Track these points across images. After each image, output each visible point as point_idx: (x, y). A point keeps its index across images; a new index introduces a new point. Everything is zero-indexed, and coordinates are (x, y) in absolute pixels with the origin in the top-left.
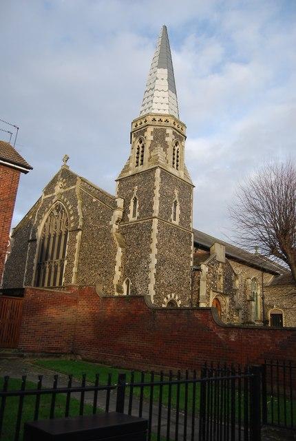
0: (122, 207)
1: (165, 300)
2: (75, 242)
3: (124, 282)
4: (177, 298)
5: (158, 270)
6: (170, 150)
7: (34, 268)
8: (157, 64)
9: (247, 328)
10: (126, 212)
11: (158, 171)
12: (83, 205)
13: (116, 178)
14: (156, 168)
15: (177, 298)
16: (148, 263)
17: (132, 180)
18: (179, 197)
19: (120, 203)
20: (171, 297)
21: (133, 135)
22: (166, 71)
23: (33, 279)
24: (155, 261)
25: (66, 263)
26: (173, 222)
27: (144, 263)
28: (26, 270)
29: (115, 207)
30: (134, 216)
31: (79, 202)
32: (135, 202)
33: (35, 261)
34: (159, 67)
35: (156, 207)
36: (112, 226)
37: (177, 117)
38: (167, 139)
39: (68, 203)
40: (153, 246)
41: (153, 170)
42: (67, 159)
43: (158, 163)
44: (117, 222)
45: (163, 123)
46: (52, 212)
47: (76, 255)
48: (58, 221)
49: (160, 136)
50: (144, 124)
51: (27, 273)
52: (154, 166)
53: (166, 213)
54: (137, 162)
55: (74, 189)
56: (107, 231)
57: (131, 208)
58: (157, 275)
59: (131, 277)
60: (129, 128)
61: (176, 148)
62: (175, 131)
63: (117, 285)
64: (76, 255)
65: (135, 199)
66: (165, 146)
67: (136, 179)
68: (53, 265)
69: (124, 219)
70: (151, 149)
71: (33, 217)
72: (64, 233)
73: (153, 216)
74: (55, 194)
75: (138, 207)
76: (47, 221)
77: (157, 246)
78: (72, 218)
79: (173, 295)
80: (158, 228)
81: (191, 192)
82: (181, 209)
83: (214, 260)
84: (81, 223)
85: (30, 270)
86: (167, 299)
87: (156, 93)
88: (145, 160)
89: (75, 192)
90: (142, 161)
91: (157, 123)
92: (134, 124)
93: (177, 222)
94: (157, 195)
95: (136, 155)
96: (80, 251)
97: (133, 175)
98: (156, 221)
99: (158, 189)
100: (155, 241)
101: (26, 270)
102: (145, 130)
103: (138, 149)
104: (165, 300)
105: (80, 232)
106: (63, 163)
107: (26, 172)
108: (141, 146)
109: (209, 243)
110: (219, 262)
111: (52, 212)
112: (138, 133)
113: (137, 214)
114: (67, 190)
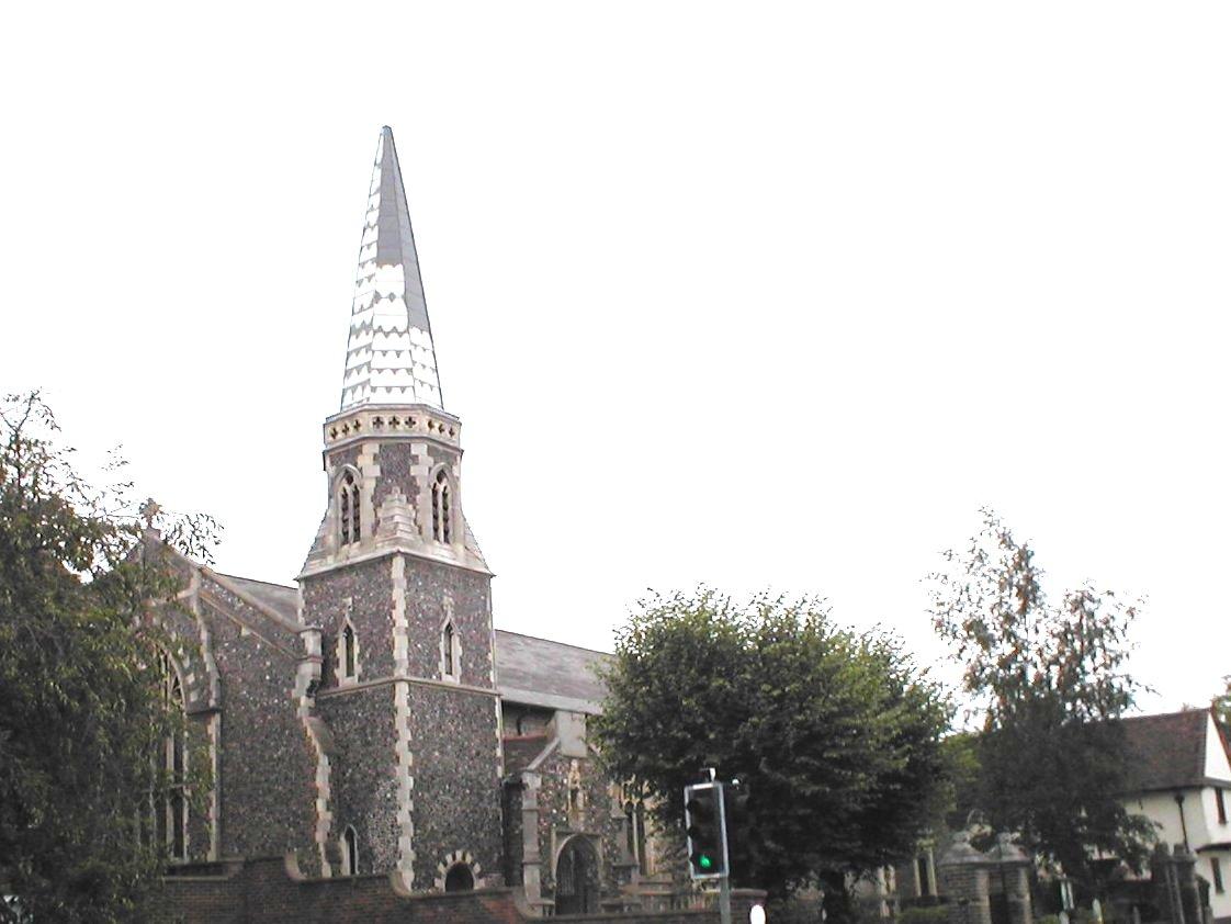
3: (343, 838)
4: (469, 859)
6: (424, 498)
8: (373, 252)
10: (328, 663)
14: (391, 556)
15: (469, 859)
16: (394, 788)
18: (455, 613)
19: (312, 644)
21: (328, 462)
24: (410, 782)
26: (448, 680)
27: (384, 786)
29: (300, 654)
30: (350, 673)
34: (380, 261)
35: (401, 651)
38: (414, 471)
40: (402, 747)
43: (397, 541)
44: (309, 691)
45: (402, 429)
49: (396, 459)
53: (424, 661)
56: (288, 714)
57: (341, 652)
58: (415, 816)
60: (317, 444)
61: (441, 488)
62: (431, 444)
63: (326, 846)
65: (348, 631)
66: (411, 489)
67: (346, 580)
69: (325, 679)
70: (377, 502)
75: (357, 650)
78: (191, 679)
79: (459, 854)
80: (410, 703)
82: (464, 643)
83: (554, 754)
86: (445, 864)
90: (357, 530)
91: (386, 430)
92: (329, 430)
93: (453, 680)
94: (402, 622)
97: (339, 571)
99: (401, 607)
100: (405, 735)
102: (359, 451)
103: (345, 496)
104: (441, 868)
105: (218, 717)
108: (349, 489)
110: (570, 758)
112: (340, 457)
113: (358, 669)
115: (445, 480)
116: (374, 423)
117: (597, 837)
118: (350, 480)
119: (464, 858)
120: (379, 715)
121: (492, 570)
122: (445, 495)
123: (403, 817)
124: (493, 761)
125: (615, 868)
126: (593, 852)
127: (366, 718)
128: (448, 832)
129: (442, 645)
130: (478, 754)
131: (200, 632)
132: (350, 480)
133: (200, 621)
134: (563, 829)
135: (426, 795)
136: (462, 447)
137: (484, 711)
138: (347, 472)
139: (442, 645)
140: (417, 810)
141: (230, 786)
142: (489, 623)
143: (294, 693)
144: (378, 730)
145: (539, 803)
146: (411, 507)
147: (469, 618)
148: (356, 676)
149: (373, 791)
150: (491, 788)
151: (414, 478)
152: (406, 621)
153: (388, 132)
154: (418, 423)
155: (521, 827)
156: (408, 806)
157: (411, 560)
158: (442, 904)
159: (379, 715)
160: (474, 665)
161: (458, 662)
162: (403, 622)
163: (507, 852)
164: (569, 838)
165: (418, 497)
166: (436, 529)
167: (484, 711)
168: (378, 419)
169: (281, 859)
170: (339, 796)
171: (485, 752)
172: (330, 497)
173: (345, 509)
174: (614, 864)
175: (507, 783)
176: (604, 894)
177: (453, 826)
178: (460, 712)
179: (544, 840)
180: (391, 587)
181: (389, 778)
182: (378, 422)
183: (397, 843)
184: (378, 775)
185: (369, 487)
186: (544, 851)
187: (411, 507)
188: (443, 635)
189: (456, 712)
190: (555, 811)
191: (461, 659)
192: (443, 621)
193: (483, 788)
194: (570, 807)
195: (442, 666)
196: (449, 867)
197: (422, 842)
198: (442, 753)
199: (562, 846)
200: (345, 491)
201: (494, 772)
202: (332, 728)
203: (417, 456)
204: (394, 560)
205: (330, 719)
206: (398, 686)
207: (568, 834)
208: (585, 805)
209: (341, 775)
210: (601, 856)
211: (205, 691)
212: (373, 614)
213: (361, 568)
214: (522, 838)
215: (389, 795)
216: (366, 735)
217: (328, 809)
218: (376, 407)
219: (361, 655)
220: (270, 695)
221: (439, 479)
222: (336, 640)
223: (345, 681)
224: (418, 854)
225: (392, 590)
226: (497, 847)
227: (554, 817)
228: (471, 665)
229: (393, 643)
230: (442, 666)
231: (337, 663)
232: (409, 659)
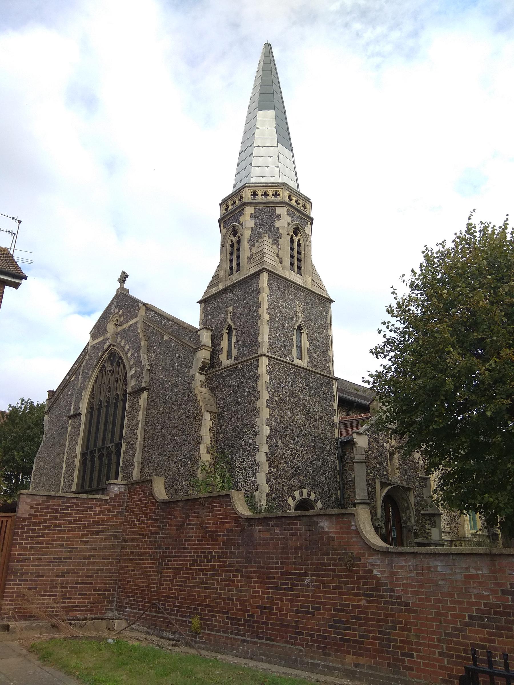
0: (210, 344)
1: (290, 501)
2: (137, 410)
4: (313, 497)
5: (272, 446)
6: (285, 242)
7: (77, 462)
9: (445, 254)
10: (215, 353)
11: (265, 277)
12: (149, 348)
13: (200, 298)
16: (255, 434)
17: (225, 298)
19: (206, 338)
20: (301, 494)
22: (271, 114)
23: (75, 481)
24: (266, 431)
25: (124, 447)
26: (297, 362)
28: (64, 466)
29: (199, 347)
31: (143, 343)
32: (230, 334)
33: (78, 450)
36: (193, 376)
37: (293, 185)
38: (278, 224)
39: (127, 347)
40: (262, 404)
41: (256, 276)
42: (124, 277)
44: (202, 369)
45: (270, 198)
46: (104, 366)
47: (139, 433)
48: (112, 379)
50: (238, 203)
51: (66, 471)
52: (256, 269)
54: (231, 268)
55: (136, 323)
57: (224, 344)
58: (270, 457)
59: (226, 463)
60: (217, 214)
61: (296, 239)
64: (139, 433)
65: (230, 329)
66: (276, 236)
67: (230, 295)
68: (105, 453)
70: (252, 243)
71: (77, 378)
72: (121, 397)
73: (260, 353)
74: (108, 335)
75: (234, 340)
76: (96, 382)
77: (269, 404)
79: (305, 491)
80: (269, 373)
81: (328, 311)
82: (311, 340)
84: (146, 378)
85: (71, 466)
86: (294, 499)
87: (256, 151)
88: (244, 261)
89: (136, 329)
90: (238, 264)
91: (260, 198)
92: (224, 206)
93: (303, 363)
95: (229, 257)
96: (146, 425)
98: (264, 362)
99: (265, 306)
100: (265, 395)
101: (64, 466)
102: (241, 213)
103: (232, 246)
104: (290, 501)
106: (118, 285)
107: (16, 286)
108: (234, 239)
109: (366, 399)
111: (104, 366)
113: (234, 352)
114: (125, 326)
115: (299, 235)
116: (252, 195)
117: (409, 489)
118: (235, 234)
119: (309, 495)
120: (247, 382)
121: (332, 297)
122: (299, 245)
123: (261, 457)
124: (332, 425)
125: (423, 514)
126: (407, 501)
127: (238, 386)
128: (297, 473)
129: (295, 338)
130: (320, 418)
131: (141, 342)
132: (235, 234)
133: (141, 335)
134: (384, 480)
135: (279, 442)
136: (312, 216)
137: (326, 389)
138: (234, 229)
139: (295, 338)
140: (272, 453)
141: (149, 440)
142: (329, 330)
143: (191, 372)
144: (246, 393)
145: (367, 458)
146: (274, 246)
147: (315, 324)
148: (233, 358)
149: (240, 438)
150: (330, 444)
151: (278, 228)
152: (268, 316)
153: (268, 47)
154: (281, 194)
155: (353, 476)
156: (265, 448)
157: (274, 276)
158: (277, 525)
159: (247, 382)
160: (318, 356)
161: (306, 352)
162: (266, 317)
163: (343, 494)
164: (392, 486)
165: (280, 240)
166: (292, 264)
167: (326, 389)
168: (254, 192)
169: (151, 481)
170: (217, 444)
171: (326, 418)
172: (222, 246)
173: (232, 254)
174: (422, 512)
175: (341, 442)
176: (416, 534)
177: (301, 469)
178: (307, 386)
179: (371, 486)
180: (258, 293)
181: (251, 428)
182: (255, 194)
183: (256, 478)
184: (244, 426)
185: (247, 234)
186: (371, 495)
187: (274, 246)
188: (295, 331)
189: (304, 386)
190: (378, 466)
191: (309, 351)
192: (296, 322)
193: (324, 444)
194: (389, 465)
195: (294, 352)
196: (296, 501)
197: (276, 479)
198: (293, 412)
199: (384, 493)
200: (232, 241)
201: (332, 432)
202: (215, 394)
203: (280, 215)
204: (261, 275)
205: (214, 389)
206: (260, 359)
207: (390, 485)
208: (400, 464)
209: (219, 428)
210: (413, 505)
211: (140, 378)
212: (246, 314)
213: (239, 286)
214: (354, 485)
215: (250, 441)
216: (237, 398)
217: (208, 453)
218: (252, 185)
219: (237, 342)
220: (177, 376)
221: (296, 233)
222: (222, 335)
223: (224, 360)
224: (271, 487)
225: (259, 295)
226: (336, 489)
227: (378, 470)
228: (316, 356)
229: (259, 331)
230: (294, 352)
231: (221, 351)
232: (269, 342)
